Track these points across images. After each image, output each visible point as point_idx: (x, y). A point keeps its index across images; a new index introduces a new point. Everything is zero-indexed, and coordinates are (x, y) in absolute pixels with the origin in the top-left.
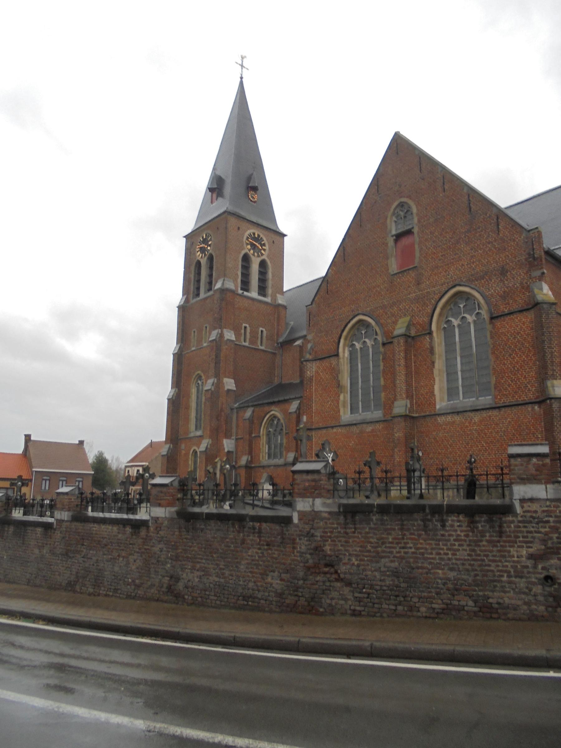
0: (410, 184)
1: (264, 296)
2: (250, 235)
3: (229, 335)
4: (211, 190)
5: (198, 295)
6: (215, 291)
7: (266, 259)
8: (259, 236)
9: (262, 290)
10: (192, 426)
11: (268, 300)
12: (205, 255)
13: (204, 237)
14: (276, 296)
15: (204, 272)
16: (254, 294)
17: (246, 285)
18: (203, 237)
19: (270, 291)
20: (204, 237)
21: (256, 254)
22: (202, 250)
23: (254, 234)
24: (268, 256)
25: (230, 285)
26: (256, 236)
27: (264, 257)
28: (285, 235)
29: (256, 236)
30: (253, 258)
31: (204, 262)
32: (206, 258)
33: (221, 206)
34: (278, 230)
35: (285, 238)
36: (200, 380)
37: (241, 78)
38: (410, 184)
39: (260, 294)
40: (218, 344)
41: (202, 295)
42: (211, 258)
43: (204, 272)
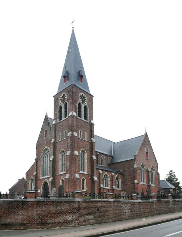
0: (171, 179)
1: (86, 120)
2: (81, 95)
3: (75, 134)
4: (65, 77)
6: (69, 117)
8: (84, 96)
11: (88, 121)
12: (63, 103)
14: (90, 120)
15: (63, 110)
16: (83, 119)
17: (80, 115)
18: (86, 102)
19: (88, 119)
22: (62, 101)
23: (82, 95)
24: (87, 104)
25: (75, 114)
27: (86, 104)
28: (93, 96)
30: (82, 104)
32: (64, 104)
33: (68, 84)
34: (89, 93)
35: (93, 97)
36: (63, 153)
38: (171, 179)
39: (85, 119)
40: (72, 137)
41: (63, 119)
42: (66, 105)
43: (63, 110)
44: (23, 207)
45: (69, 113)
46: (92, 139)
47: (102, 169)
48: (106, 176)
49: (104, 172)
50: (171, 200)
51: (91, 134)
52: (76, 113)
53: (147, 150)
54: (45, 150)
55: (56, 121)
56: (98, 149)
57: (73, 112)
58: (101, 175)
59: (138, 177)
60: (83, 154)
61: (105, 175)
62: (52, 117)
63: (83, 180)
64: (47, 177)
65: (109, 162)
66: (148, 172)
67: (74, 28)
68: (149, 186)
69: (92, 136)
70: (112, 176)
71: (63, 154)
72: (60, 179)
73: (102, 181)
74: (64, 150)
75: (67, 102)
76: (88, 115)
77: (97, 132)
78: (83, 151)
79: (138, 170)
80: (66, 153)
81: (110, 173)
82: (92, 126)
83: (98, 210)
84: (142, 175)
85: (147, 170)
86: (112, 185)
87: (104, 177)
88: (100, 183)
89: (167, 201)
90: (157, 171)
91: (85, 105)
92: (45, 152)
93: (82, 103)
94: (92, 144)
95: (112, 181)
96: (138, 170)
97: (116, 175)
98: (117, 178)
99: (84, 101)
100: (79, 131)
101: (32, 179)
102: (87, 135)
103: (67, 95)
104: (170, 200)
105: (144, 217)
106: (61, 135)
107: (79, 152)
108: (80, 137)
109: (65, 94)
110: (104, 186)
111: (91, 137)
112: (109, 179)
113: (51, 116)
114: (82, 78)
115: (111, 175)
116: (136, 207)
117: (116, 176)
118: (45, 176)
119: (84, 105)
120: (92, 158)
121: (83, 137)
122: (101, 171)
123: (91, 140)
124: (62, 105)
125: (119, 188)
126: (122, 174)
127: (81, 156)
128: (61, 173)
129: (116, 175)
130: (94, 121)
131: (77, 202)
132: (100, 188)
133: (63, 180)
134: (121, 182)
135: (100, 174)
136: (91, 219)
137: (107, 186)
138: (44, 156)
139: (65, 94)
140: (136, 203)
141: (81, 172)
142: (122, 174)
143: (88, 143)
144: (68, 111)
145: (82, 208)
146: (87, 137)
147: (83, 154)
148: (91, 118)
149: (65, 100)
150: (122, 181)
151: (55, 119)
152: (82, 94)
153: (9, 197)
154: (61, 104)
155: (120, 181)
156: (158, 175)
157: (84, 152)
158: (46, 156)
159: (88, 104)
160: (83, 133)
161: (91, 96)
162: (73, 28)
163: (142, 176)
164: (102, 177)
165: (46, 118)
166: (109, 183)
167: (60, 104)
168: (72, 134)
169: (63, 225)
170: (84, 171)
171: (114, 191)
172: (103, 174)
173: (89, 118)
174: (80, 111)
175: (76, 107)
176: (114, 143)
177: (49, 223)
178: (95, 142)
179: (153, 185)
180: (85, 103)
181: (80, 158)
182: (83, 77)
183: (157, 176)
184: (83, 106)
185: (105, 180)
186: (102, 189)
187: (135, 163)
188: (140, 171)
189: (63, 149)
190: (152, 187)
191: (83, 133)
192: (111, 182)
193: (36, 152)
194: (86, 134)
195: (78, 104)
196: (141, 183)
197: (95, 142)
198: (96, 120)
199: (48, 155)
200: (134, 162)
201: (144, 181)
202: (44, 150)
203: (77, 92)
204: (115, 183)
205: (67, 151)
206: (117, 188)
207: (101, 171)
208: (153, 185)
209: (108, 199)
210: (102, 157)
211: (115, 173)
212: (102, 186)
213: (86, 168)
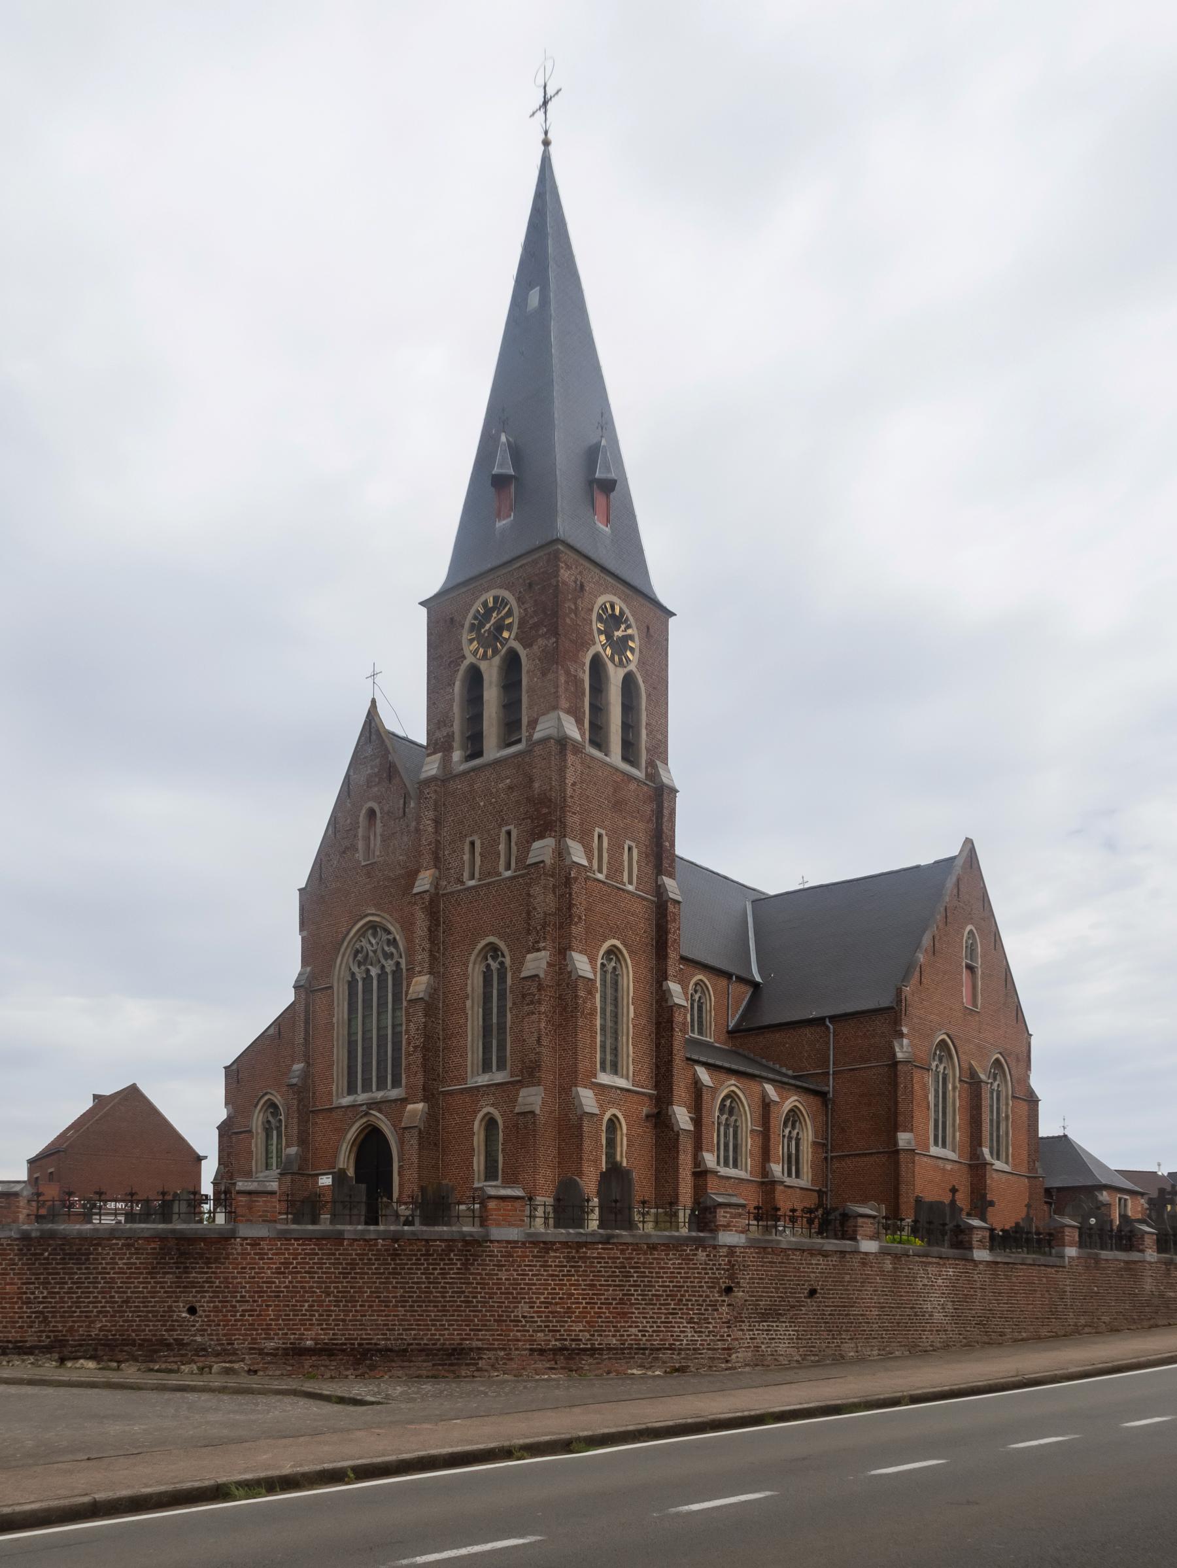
5: (478, 753)
6: (532, 745)
7: (635, 670)
9: (629, 750)
10: (339, 1080)
11: (639, 774)
13: (629, 654)
14: (655, 767)
15: (491, 695)
16: (615, 756)
18: (632, 650)
20: (629, 654)
21: (616, 658)
25: (572, 730)
26: (617, 612)
27: (632, 667)
29: (617, 612)
31: (491, 671)
32: (497, 660)
34: (636, 582)
35: (672, 621)
36: (494, 958)
37: (546, 143)
39: (625, 758)
42: (512, 663)
43: (491, 695)
44: (467, 1269)
45: (533, 723)
46: (667, 881)
47: (711, 1061)
48: (730, 1106)
49: (723, 1076)
50: (1151, 1255)
51: (660, 851)
52: (579, 722)
53: (972, 950)
54: (364, 935)
55: (446, 762)
56: (693, 936)
57: (563, 715)
58: (706, 1097)
59: (917, 1114)
60: (610, 967)
61: (724, 1100)
62: (418, 733)
63: (613, 1123)
64: (379, 1095)
65: (733, 1016)
66: (974, 1085)
67: (552, 148)
68: (977, 1168)
69: (665, 864)
70: (766, 1106)
71: (494, 965)
72: (476, 1112)
73: (712, 1136)
74: (502, 945)
75: (523, 653)
76: (644, 732)
77: (691, 843)
78: (612, 952)
79: (917, 1075)
80: (519, 963)
81: (754, 1087)
82: (660, 800)
83: (813, 1293)
84: (936, 1105)
85: (973, 1074)
86: (765, 1155)
87: (722, 1110)
88: (698, 1147)
89: (1129, 1265)
90: (1024, 1080)
91: (626, 670)
92: (364, 943)
93: (612, 659)
94: (662, 913)
95: (765, 1135)
96: (917, 1075)
97: (784, 1099)
98: (793, 1117)
99: (620, 646)
100: (591, 832)
101: (273, 1105)
102: (633, 857)
103: (520, 601)
104: (1148, 1259)
105: (1016, 1341)
106: (478, 849)
107: (592, 960)
108: (600, 871)
109: (506, 594)
110: (718, 1163)
111: (659, 870)
112: (748, 1121)
113: (410, 720)
114: (608, 497)
115: (757, 1099)
116: (978, 1285)
117: (788, 1105)
118: (381, 1085)
119: (621, 673)
120: (662, 996)
121: (615, 870)
122: (704, 1075)
123: (660, 890)
124: (483, 666)
125: (797, 1176)
126: (822, 1095)
127: (604, 981)
128: (483, 1080)
129: (787, 1099)
130: (679, 769)
131: (725, 1250)
132: (701, 1174)
133: (491, 1123)
134: (814, 1143)
135: (697, 1088)
136: (782, 1339)
137: (735, 1166)
138: (355, 969)
139: (506, 594)
140: (981, 1267)
141: (604, 1078)
142: (822, 1095)
143: (639, 908)
144: (530, 707)
145: (744, 1279)
146: (605, 855)
147: (610, 967)
148: (660, 750)
149: (506, 634)
150: (816, 1136)
151: (438, 742)
152: (615, 599)
153: (175, 1217)
154: (475, 653)
155: (808, 1135)
156: (1032, 1101)
157: (618, 960)
158: (374, 972)
159: (642, 663)
160: (616, 848)
161: (659, 613)
162: (546, 143)
163: (936, 1111)
164: (713, 1113)
165: (372, 727)
166: (749, 1143)
167: (470, 659)
168: (561, 853)
169: (657, 1359)
170: (615, 1070)
171: (773, 1191)
172: (714, 1090)
173: (648, 750)
174: (598, 710)
175: (578, 682)
176: (761, 901)
177: (593, 1351)
178: (679, 902)
179: (999, 1165)
180: (627, 658)
181: (598, 996)
182: (613, 489)
183: (1023, 1108)
184: (616, 676)
185: (727, 1125)
186: (779, 1188)
187: (905, 1030)
188: (930, 1081)
189: (491, 939)
190: (995, 1175)
191: (616, 848)
192: (759, 1141)
193: (303, 939)
194: (630, 849)
195: (587, 668)
196: (934, 1151)
197: (679, 898)
198: (691, 760)
199: (389, 966)
200: (896, 1022)
201: (949, 1140)
202: (362, 933)
203: (582, 586)
204: (779, 1149)
205: (522, 949)
206: (790, 1175)
207: (704, 1075)
208: (999, 1165)
209: (854, 1239)
210: (696, 984)
211: (779, 1084)
212: (710, 1159)
213: (629, 1051)
